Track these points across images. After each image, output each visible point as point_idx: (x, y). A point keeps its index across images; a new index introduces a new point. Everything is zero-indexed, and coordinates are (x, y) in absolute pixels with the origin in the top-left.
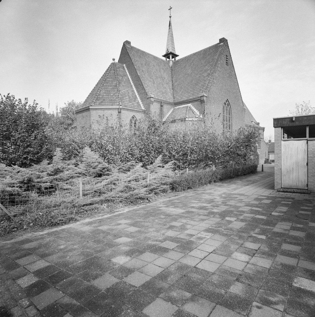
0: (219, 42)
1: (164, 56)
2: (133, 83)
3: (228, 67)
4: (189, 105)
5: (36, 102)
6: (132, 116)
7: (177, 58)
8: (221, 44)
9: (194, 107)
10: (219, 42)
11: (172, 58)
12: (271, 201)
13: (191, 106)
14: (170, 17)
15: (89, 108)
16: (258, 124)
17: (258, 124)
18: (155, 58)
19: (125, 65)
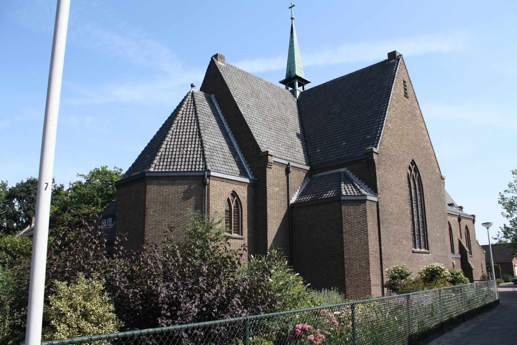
0: (387, 58)
1: (282, 82)
2: (229, 128)
3: (408, 102)
4: (343, 170)
5: (507, 188)
6: (230, 191)
7: (307, 87)
8: (391, 61)
9: (353, 174)
10: (387, 58)
11: (299, 86)
12: (194, 198)
13: (348, 172)
14: (292, 19)
15: (145, 174)
16: (461, 208)
17: (461, 208)
18: (269, 85)
19: (213, 96)
